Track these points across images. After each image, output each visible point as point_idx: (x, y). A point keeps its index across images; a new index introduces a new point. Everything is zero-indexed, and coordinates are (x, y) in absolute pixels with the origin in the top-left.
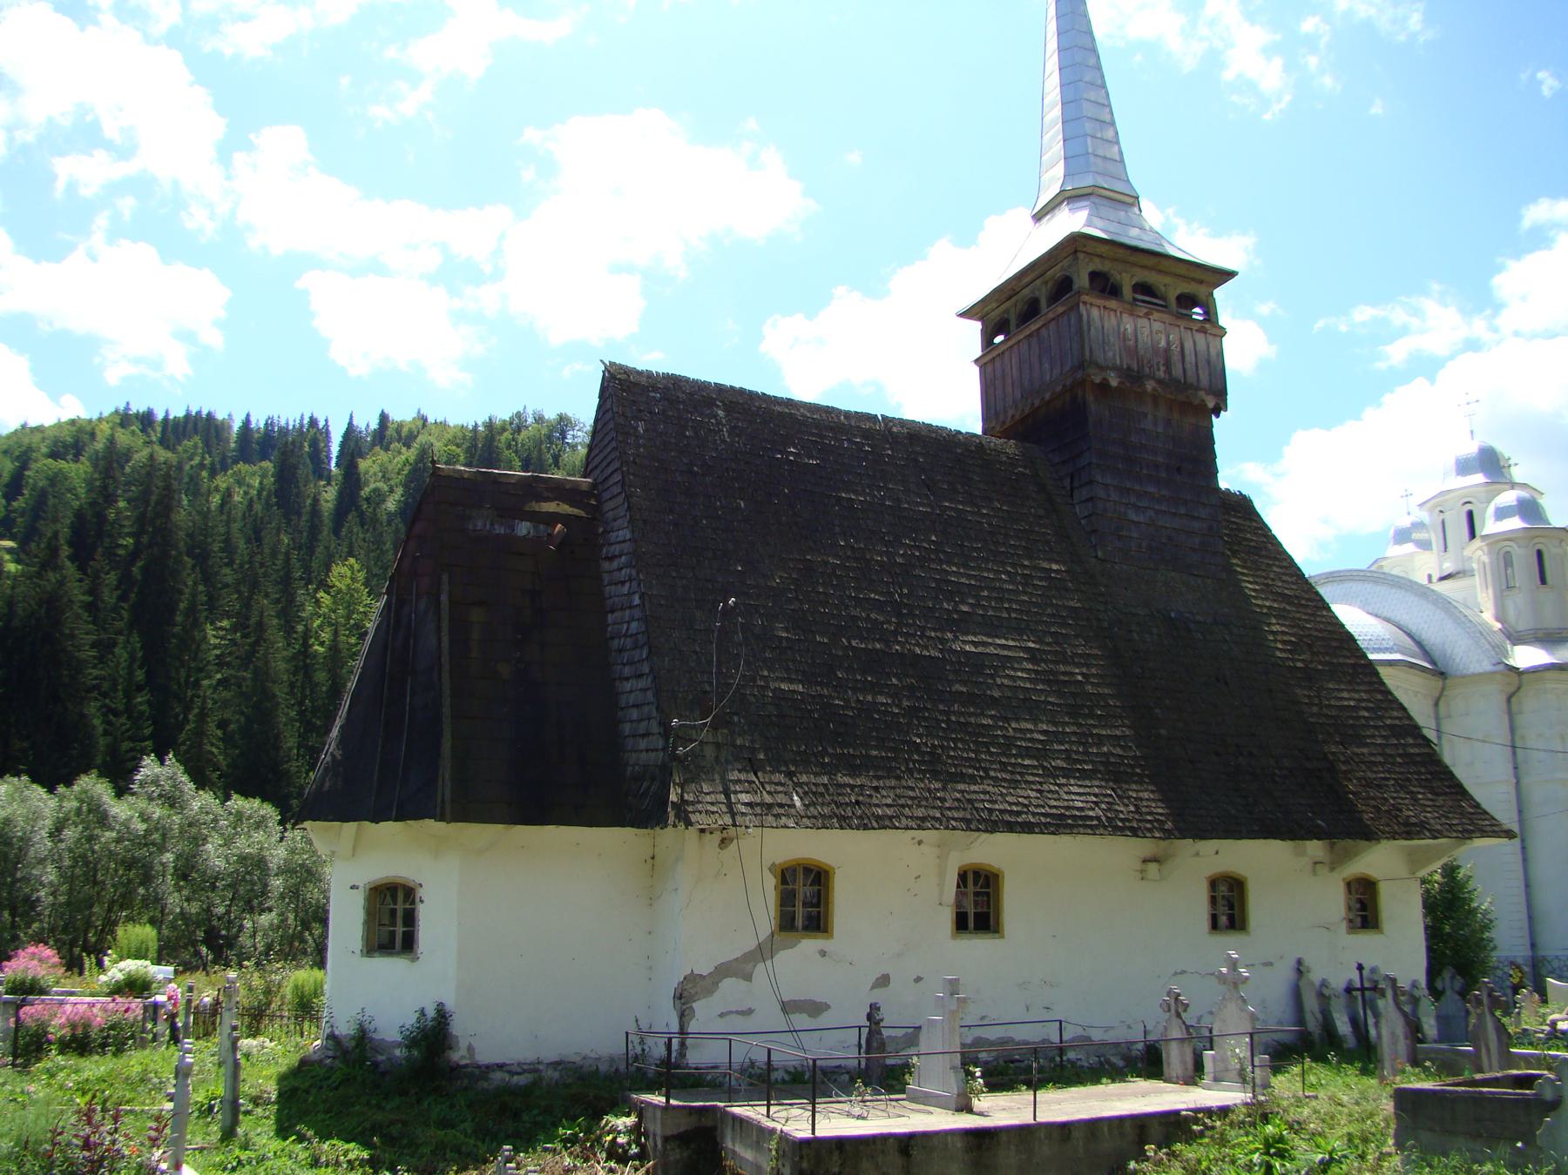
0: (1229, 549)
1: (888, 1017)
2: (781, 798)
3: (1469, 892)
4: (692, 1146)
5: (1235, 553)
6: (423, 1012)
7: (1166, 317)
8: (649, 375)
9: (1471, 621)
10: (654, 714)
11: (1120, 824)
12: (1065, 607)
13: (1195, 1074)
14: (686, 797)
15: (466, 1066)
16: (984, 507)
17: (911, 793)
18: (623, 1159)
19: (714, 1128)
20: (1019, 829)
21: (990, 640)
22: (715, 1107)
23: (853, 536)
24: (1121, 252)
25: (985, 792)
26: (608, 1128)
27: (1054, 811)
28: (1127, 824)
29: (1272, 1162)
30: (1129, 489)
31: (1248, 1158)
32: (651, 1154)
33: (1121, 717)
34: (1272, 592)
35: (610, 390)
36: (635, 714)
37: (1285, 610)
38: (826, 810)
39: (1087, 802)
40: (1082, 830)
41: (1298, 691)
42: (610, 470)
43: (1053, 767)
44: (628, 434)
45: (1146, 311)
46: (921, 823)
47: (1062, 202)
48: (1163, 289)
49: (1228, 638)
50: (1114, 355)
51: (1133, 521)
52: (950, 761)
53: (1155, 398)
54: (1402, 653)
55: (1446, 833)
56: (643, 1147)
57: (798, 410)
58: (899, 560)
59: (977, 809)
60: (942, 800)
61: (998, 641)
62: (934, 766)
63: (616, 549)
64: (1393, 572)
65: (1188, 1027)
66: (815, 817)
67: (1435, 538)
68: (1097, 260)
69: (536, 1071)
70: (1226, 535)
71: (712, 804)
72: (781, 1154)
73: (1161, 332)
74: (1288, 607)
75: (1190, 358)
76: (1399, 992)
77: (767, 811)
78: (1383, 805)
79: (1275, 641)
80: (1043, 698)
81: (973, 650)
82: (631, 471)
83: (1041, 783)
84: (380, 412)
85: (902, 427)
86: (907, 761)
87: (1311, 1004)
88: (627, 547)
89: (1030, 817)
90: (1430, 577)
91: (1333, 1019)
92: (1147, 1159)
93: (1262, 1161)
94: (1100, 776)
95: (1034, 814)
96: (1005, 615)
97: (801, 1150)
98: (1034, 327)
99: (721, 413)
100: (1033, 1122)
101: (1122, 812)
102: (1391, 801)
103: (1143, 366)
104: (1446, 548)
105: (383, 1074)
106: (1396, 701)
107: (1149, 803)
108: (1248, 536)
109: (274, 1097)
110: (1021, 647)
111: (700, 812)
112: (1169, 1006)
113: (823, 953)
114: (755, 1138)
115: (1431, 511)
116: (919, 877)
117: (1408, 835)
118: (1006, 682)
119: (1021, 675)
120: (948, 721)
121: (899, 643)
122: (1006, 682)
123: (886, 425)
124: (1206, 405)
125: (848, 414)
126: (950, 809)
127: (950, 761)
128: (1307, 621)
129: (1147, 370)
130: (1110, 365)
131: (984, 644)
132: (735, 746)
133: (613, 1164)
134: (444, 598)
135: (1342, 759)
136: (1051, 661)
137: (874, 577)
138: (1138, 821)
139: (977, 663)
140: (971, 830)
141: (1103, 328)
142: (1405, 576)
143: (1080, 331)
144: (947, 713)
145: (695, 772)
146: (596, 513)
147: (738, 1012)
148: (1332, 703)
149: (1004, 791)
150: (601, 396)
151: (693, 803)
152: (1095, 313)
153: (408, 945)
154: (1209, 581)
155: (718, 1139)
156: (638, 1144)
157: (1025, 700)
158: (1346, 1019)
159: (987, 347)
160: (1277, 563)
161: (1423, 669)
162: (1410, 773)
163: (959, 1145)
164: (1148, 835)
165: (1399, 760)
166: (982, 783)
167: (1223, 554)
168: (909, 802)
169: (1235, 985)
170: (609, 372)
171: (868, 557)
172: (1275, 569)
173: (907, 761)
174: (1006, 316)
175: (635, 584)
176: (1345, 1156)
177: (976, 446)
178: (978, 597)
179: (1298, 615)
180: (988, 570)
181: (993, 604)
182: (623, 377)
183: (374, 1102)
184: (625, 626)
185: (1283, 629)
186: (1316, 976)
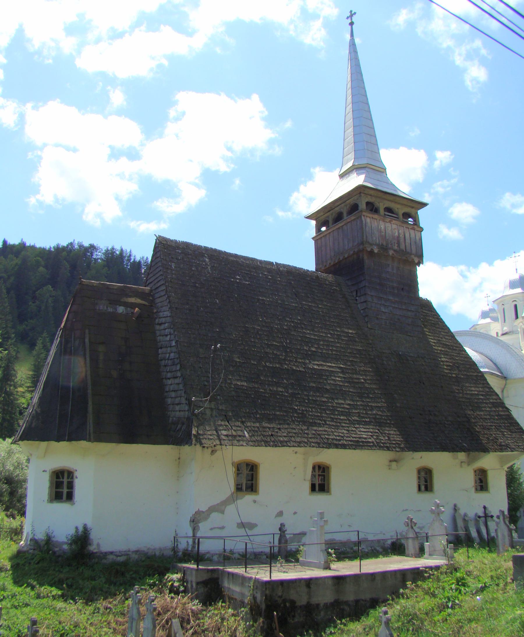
0: (423, 325)
1: (290, 530)
2: (240, 433)
3: (519, 475)
4: (209, 586)
5: (425, 326)
6: (77, 528)
7: (399, 223)
8: (176, 242)
9: (518, 354)
10: (183, 395)
11: (382, 445)
12: (356, 349)
13: (421, 552)
14: (199, 432)
15: (96, 553)
16: (320, 304)
17: (294, 431)
18: (177, 593)
19: (218, 579)
20: (340, 447)
21: (324, 364)
22: (218, 569)
23: (265, 316)
24: (380, 194)
25: (325, 431)
26: (169, 579)
27: (354, 439)
28: (385, 445)
29: (460, 588)
30: (382, 298)
31: (450, 586)
32: (190, 590)
33: (380, 398)
34: (441, 343)
35: (159, 248)
36: (173, 394)
37: (447, 351)
38: (259, 438)
39: (368, 435)
40: (366, 448)
41: (454, 387)
42: (159, 284)
43: (353, 420)
44: (167, 268)
45: (390, 219)
46: (299, 444)
47: (353, 170)
48: (397, 210)
49: (423, 363)
50: (376, 239)
51: (383, 312)
52: (310, 417)
53: (393, 258)
54: (488, 368)
55: (517, 449)
56: (185, 587)
57: (240, 260)
58: (285, 327)
59: (322, 438)
60: (307, 434)
61: (328, 364)
62: (303, 419)
63: (163, 320)
64: (481, 331)
65: (416, 533)
66: (255, 441)
67: (500, 316)
68: (369, 197)
69: (127, 555)
70: (422, 318)
71: (211, 435)
72: (255, 588)
73: (395, 229)
74: (448, 350)
75: (408, 241)
76: (505, 517)
77: (235, 439)
78: (490, 437)
79: (443, 365)
80: (347, 390)
81: (317, 368)
82: (170, 285)
83: (348, 427)
84: (3, 239)
85: (284, 268)
86: (292, 417)
87: (460, 524)
88: (168, 319)
89: (344, 442)
90: (497, 333)
91: (481, 529)
92: (407, 588)
93: (456, 588)
94: (372, 424)
95: (346, 440)
96: (330, 352)
97: (266, 585)
98: (340, 225)
99: (207, 260)
100: (359, 573)
101: (383, 440)
102: (494, 435)
103: (388, 244)
104: (505, 320)
105: (59, 556)
106: (494, 391)
107: (394, 436)
108: (431, 318)
109: (9, 567)
110: (337, 367)
111: (206, 439)
112: (408, 524)
113: (255, 502)
114: (240, 581)
115: (498, 305)
116: (296, 468)
117: (501, 450)
118: (332, 382)
119: (338, 379)
120: (308, 399)
121: (286, 364)
122: (332, 382)
123: (277, 267)
124: (414, 261)
125: (261, 262)
126: (311, 438)
127: (310, 417)
128: (456, 356)
129: (390, 246)
130: (374, 243)
131: (322, 365)
132: (219, 409)
133: (173, 595)
134: (87, 340)
135: (473, 417)
136: (351, 373)
137: (275, 335)
138: (389, 443)
139: (319, 374)
140: (320, 447)
141: (371, 226)
142: (487, 333)
143: (362, 228)
144: (307, 396)
145: (202, 421)
146: (152, 304)
147: (218, 528)
148: (468, 392)
149: (333, 430)
150: (154, 251)
151: (202, 435)
152: (368, 220)
153: (70, 497)
154: (415, 338)
155: (220, 583)
156: (184, 586)
157: (340, 390)
158: (475, 530)
159: (318, 233)
160: (443, 330)
161: (497, 376)
162: (501, 423)
163: (330, 583)
164: (394, 450)
165: (496, 417)
166: (324, 427)
167: (421, 326)
168: (294, 435)
169: (438, 514)
170: (159, 240)
171: (272, 326)
172: (442, 333)
173: (292, 417)
174: (327, 219)
175: (172, 336)
176: (491, 585)
177: (316, 277)
178: (318, 344)
179: (452, 354)
180: (322, 332)
181: (325, 347)
182: (165, 242)
183: (57, 569)
184: (168, 355)
185: (447, 360)
186: (462, 512)
